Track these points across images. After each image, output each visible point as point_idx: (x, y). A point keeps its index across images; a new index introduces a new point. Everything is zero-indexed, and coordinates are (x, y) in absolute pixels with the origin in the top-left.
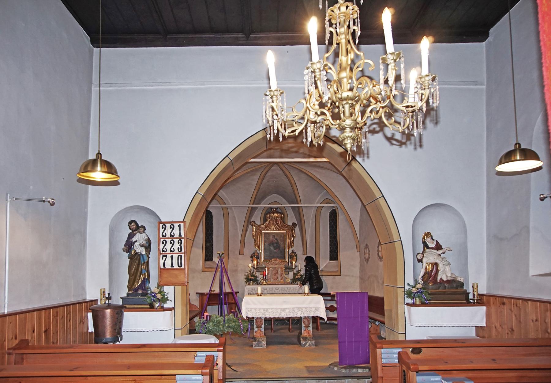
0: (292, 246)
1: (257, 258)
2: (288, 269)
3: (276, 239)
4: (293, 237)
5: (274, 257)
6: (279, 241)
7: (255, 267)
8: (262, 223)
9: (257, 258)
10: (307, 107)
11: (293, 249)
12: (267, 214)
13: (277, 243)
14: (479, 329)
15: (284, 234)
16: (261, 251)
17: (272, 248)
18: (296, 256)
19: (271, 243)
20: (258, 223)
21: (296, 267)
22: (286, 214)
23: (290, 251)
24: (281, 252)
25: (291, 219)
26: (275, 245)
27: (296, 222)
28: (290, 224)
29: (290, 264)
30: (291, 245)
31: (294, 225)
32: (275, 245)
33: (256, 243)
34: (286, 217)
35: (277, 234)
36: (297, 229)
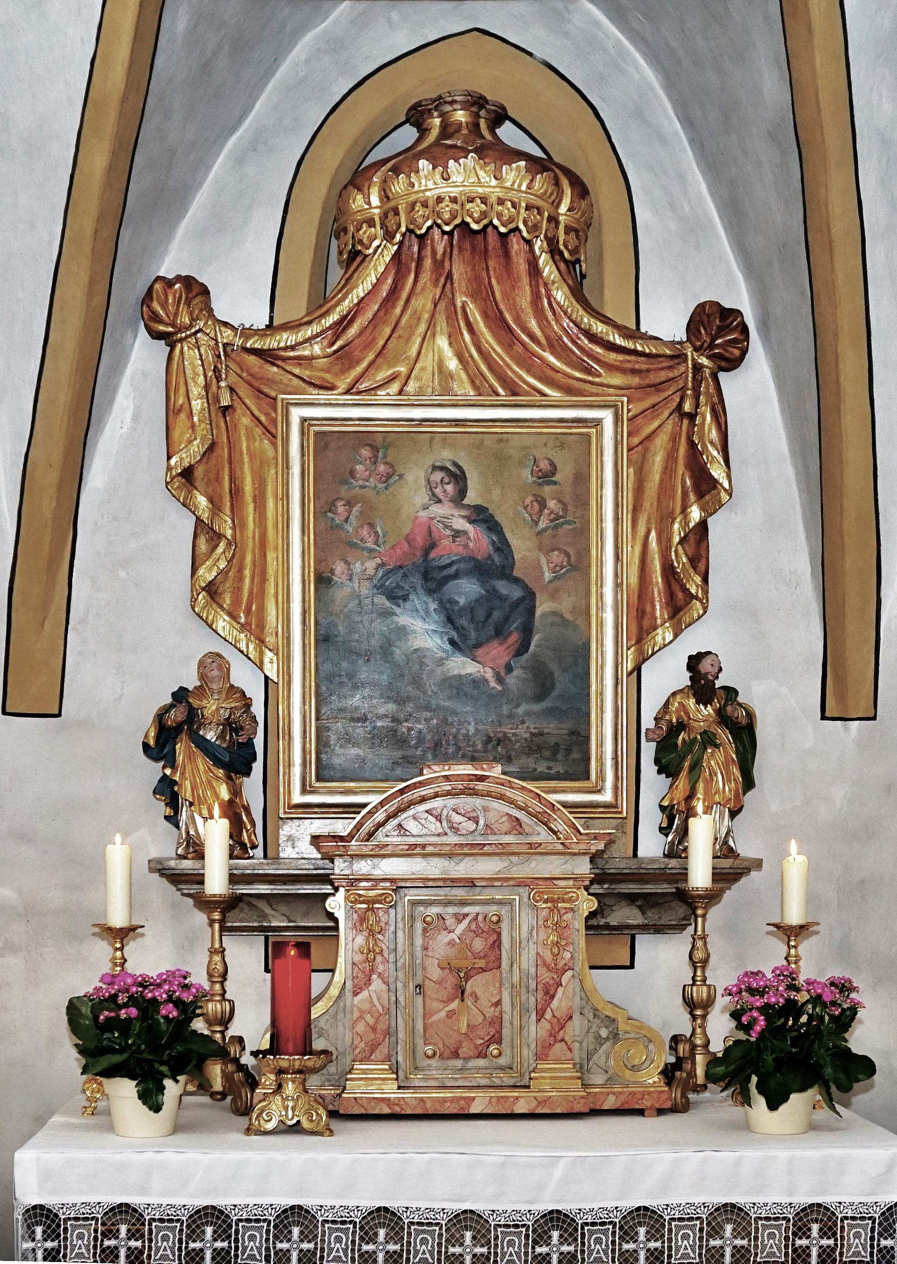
0: (681, 605)
1: (236, 760)
2: (643, 900)
3: (481, 516)
4: (705, 486)
5: (441, 748)
6: (522, 545)
7: (216, 883)
8: (294, 306)
9: (236, 760)
10: (538, 953)
11: (694, 640)
12: (358, 179)
13: (496, 566)
14: (667, 777)
15: (582, 437)
16: (276, 675)
17: (422, 631)
18: (744, 734)
19: (423, 572)
20: (242, 302)
21: (731, 869)
22: (605, 192)
23: (665, 677)
24: (542, 685)
25: (680, 266)
26: (467, 590)
27: (740, 298)
28: (666, 319)
29: (652, 845)
30: (675, 589)
31: (718, 332)
32: (467, 590)
33: (227, 589)
34: (612, 233)
35: (494, 444)
36: (754, 394)
